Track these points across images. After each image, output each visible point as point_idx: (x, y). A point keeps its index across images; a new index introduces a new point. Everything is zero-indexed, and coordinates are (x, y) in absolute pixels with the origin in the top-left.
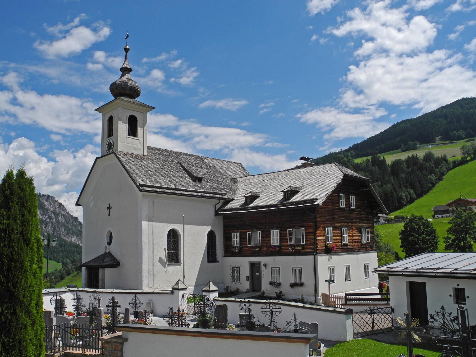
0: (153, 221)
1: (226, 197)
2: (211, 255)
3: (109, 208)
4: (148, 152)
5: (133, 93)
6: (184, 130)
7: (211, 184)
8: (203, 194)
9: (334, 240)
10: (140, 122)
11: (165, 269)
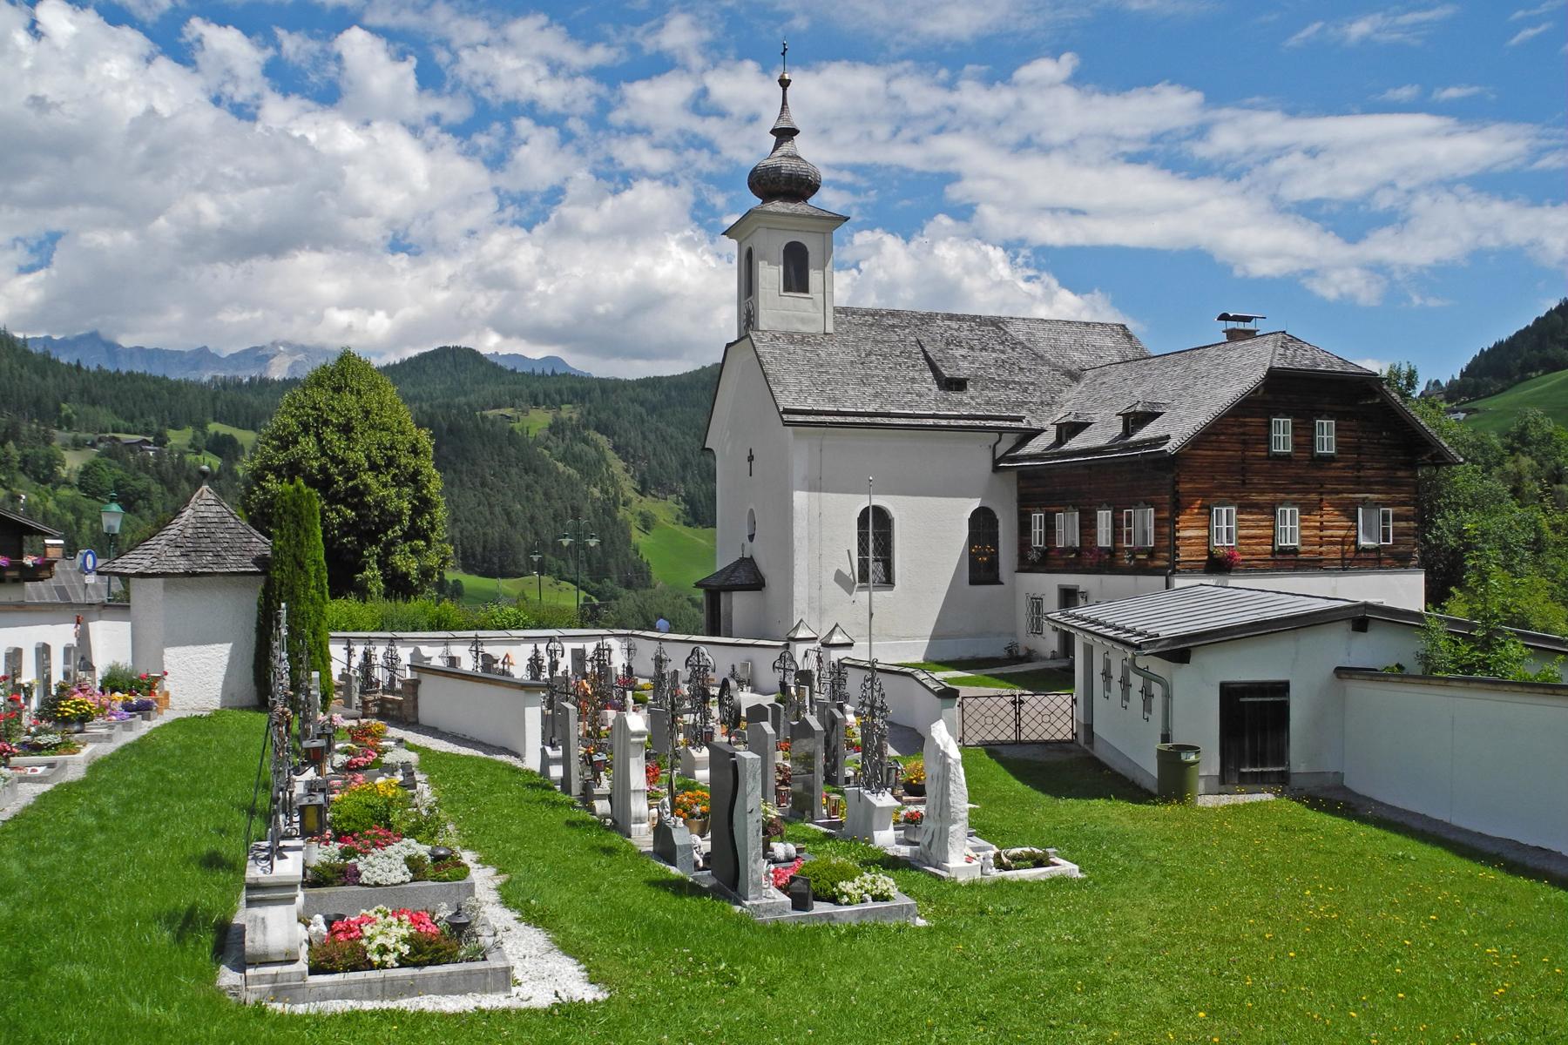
1: (1022, 425)
2: (981, 567)
3: (751, 458)
4: (837, 323)
5: (798, 187)
6: (1228, 138)
7: (991, 394)
8: (953, 422)
9: (1241, 537)
10: (813, 259)
11: (853, 597)
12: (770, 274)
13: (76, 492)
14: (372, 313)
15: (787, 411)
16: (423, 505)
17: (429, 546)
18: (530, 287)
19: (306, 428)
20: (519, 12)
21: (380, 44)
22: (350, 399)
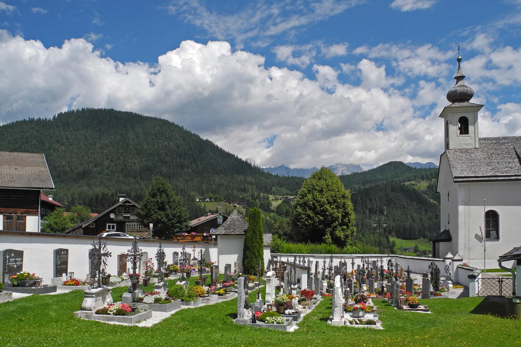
0: (469, 205)
4: (480, 144)
5: (466, 96)
12: (455, 129)
13: (275, 214)
14: (370, 152)
15: (455, 177)
16: (346, 215)
17: (348, 228)
18: (423, 138)
19: (309, 192)
20: (421, 44)
21: (373, 63)
22: (322, 182)
